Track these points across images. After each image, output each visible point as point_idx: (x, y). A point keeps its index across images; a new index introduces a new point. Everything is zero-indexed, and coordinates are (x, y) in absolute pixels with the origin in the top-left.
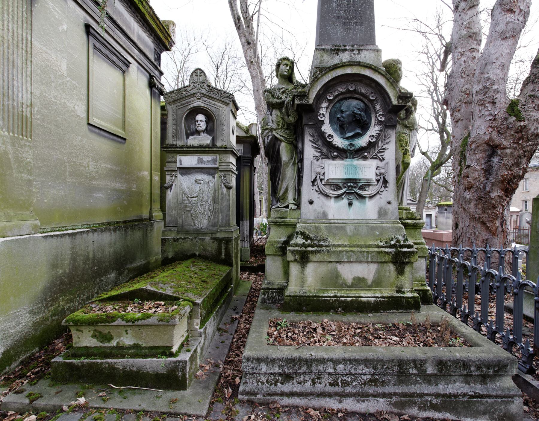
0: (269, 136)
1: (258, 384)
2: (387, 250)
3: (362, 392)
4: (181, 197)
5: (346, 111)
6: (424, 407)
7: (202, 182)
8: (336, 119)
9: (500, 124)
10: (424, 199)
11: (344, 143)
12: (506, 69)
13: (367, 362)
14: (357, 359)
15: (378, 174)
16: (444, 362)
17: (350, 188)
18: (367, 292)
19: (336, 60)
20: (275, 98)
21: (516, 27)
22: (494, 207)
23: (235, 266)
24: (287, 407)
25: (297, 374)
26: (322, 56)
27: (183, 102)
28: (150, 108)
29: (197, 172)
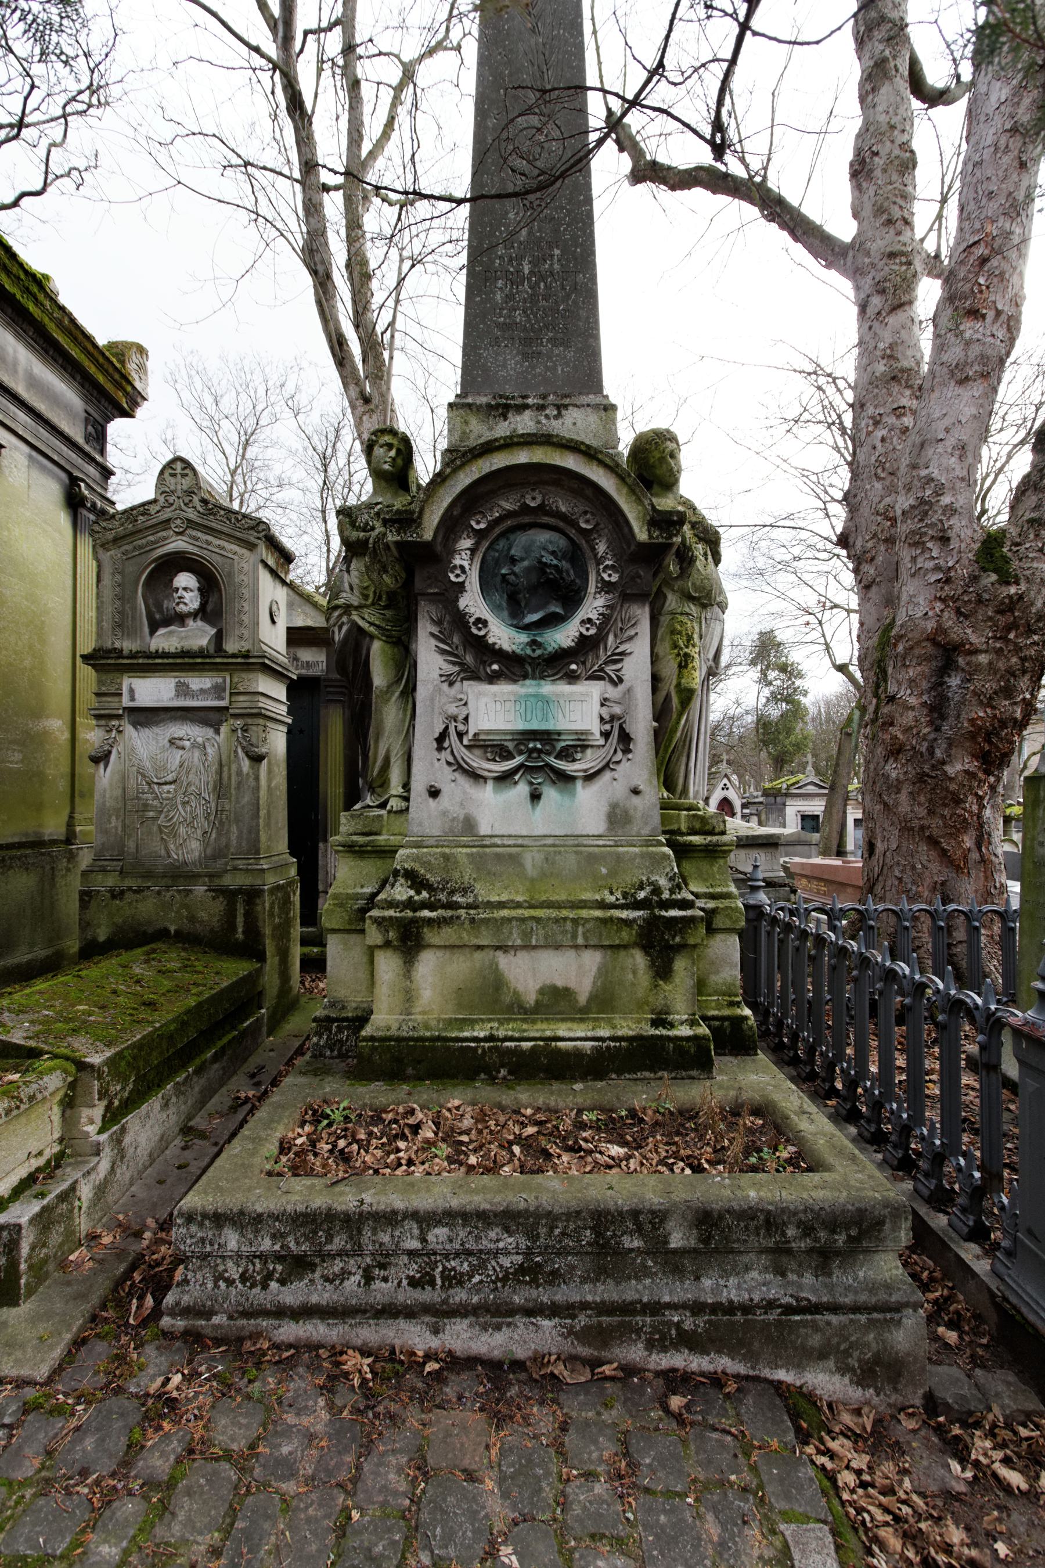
0: (343, 624)
1: (216, 1286)
2: (624, 914)
3: (494, 1303)
4: (132, 783)
5: (522, 559)
6: (663, 1339)
7: (187, 744)
8: (499, 579)
9: (960, 592)
10: (845, 782)
11: (517, 641)
12: (970, 455)
13: (508, 1219)
14: (484, 1212)
15: (607, 717)
16: (715, 1214)
17: (535, 755)
18: (575, 1026)
19: (502, 429)
20: (358, 529)
21: (990, 352)
22: (958, 801)
23: (272, 960)
24: (290, 1346)
25: (326, 1257)
26: (466, 423)
27: (140, 542)
28: (69, 559)
29: (174, 719)
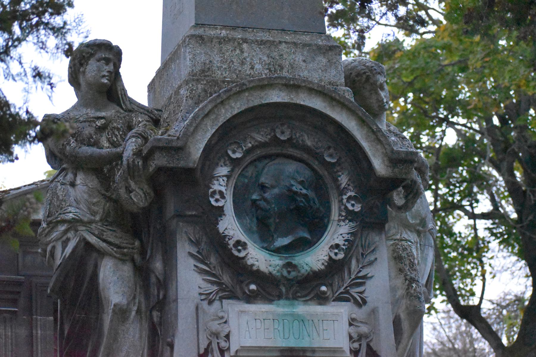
5: (273, 187)
8: (249, 203)
15: (355, 336)
